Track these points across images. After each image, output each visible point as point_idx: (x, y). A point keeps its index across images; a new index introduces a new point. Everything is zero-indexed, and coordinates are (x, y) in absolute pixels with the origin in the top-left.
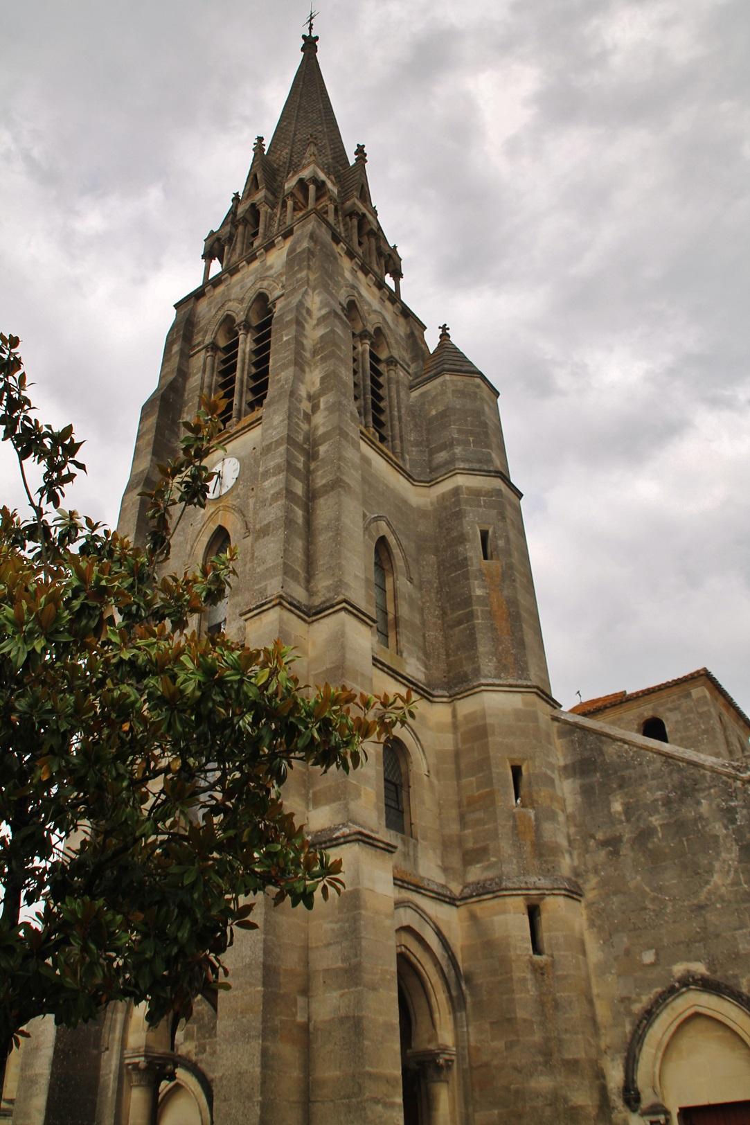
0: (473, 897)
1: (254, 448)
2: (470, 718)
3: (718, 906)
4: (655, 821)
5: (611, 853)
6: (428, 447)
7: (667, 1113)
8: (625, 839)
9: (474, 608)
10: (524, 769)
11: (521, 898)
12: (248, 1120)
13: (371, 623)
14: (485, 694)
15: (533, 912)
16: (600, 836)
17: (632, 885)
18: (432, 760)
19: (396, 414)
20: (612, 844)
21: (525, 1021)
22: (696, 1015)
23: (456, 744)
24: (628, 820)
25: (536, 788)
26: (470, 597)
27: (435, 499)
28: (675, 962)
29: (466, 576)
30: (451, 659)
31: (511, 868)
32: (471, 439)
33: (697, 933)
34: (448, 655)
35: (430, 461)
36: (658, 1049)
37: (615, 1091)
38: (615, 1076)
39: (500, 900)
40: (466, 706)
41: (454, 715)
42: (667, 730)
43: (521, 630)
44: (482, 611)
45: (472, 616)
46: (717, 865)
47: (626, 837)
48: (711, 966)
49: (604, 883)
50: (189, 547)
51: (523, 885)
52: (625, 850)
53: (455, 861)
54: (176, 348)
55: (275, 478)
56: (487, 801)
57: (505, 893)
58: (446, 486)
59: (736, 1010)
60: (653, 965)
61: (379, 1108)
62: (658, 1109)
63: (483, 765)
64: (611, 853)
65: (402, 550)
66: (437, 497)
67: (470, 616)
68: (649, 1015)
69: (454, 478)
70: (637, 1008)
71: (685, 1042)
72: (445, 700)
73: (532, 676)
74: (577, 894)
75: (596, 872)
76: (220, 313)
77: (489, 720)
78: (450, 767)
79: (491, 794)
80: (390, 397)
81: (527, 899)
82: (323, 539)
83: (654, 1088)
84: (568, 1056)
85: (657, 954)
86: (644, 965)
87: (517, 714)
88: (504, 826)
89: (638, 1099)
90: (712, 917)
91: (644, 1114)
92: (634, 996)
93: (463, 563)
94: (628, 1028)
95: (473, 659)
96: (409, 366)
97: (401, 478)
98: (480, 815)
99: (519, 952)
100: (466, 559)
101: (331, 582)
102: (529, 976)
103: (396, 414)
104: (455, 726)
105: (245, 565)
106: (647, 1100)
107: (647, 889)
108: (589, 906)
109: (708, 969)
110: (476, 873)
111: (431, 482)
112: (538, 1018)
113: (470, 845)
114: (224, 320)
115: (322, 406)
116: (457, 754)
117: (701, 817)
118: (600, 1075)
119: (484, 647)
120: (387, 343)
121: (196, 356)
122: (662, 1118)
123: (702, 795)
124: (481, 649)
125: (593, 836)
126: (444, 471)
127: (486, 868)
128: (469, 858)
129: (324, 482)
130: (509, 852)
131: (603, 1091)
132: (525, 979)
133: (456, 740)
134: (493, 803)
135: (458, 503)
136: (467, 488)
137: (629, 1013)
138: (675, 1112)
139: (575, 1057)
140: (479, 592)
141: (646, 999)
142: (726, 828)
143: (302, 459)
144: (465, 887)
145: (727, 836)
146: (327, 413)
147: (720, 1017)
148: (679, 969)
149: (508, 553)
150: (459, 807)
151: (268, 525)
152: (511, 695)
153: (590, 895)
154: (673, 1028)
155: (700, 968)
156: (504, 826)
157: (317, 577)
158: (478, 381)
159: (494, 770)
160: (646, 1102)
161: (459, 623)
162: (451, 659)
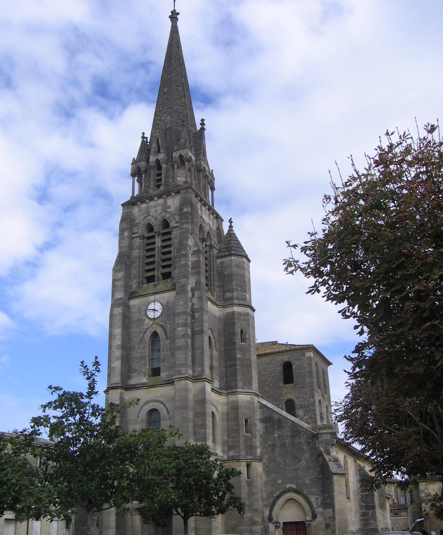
0: (230, 460)
1: (168, 302)
2: (233, 402)
3: (302, 469)
4: (287, 441)
5: (272, 449)
6: (223, 289)
7: (279, 523)
8: (277, 445)
9: (237, 362)
10: (249, 421)
11: (245, 462)
12: (88, 369)
13: (211, 382)
14: (239, 395)
15: (248, 466)
16: (269, 443)
17: (278, 460)
18: (220, 416)
19: (212, 273)
20: (273, 446)
21: (244, 498)
22: (291, 499)
23: (228, 410)
25: (252, 427)
26: (236, 357)
28: (287, 484)
29: (235, 349)
30: (227, 379)
31: (243, 453)
32: (240, 288)
33: (294, 476)
34: (226, 378)
35: (224, 295)
36: (279, 507)
37: (266, 517)
38: (267, 513)
39: (239, 463)
40: (232, 398)
41: (228, 400)
44: (239, 363)
45: (236, 365)
46: (303, 458)
47: (278, 445)
50: (142, 335)
51: (246, 459)
53: (226, 449)
55: (182, 328)
56: (237, 431)
57: (241, 461)
58: (229, 310)
59: (302, 498)
60: (281, 484)
62: (277, 522)
63: (237, 419)
64: (272, 449)
65: (214, 339)
66: (226, 313)
67: (235, 365)
68: (278, 497)
69: (233, 308)
70: (275, 495)
71: (287, 505)
72: (225, 394)
73: (254, 388)
74: (261, 460)
75: (267, 454)
77: (239, 404)
79: (239, 429)
80: (210, 264)
81: (247, 463)
82: (197, 352)
84: (255, 508)
86: (278, 483)
88: (242, 439)
89: (272, 520)
90: (299, 473)
91: (273, 523)
92: (274, 492)
93: (234, 344)
95: (235, 380)
96: (217, 245)
97: (214, 306)
98: (234, 435)
99: (244, 478)
100: (235, 342)
101: (201, 369)
103: (212, 273)
104: (228, 404)
105: (167, 351)
106: (275, 520)
108: (264, 464)
109: (296, 487)
110: (232, 453)
111: (224, 306)
112: (248, 497)
115: (196, 296)
116: (228, 413)
117: (300, 443)
123: (301, 436)
124: (238, 378)
127: (236, 452)
128: (230, 448)
130: (243, 448)
132: (244, 486)
133: (228, 409)
134: (239, 432)
135: (233, 318)
136: (238, 312)
137: (273, 496)
138: (282, 523)
139: (257, 508)
140: (239, 356)
141: (278, 493)
142: (307, 447)
143: (190, 319)
144: (228, 457)
145: (307, 450)
147: (297, 500)
148: (288, 486)
149: (249, 340)
150: (228, 431)
152: (246, 395)
153: (265, 461)
154: (284, 502)
155: (294, 486)
156: (242, 439)
157: (195, 366)
158: (245, 260)
159: (240, 421)
160: (274, 520)
161: (231, 367)
162: (227, 379)
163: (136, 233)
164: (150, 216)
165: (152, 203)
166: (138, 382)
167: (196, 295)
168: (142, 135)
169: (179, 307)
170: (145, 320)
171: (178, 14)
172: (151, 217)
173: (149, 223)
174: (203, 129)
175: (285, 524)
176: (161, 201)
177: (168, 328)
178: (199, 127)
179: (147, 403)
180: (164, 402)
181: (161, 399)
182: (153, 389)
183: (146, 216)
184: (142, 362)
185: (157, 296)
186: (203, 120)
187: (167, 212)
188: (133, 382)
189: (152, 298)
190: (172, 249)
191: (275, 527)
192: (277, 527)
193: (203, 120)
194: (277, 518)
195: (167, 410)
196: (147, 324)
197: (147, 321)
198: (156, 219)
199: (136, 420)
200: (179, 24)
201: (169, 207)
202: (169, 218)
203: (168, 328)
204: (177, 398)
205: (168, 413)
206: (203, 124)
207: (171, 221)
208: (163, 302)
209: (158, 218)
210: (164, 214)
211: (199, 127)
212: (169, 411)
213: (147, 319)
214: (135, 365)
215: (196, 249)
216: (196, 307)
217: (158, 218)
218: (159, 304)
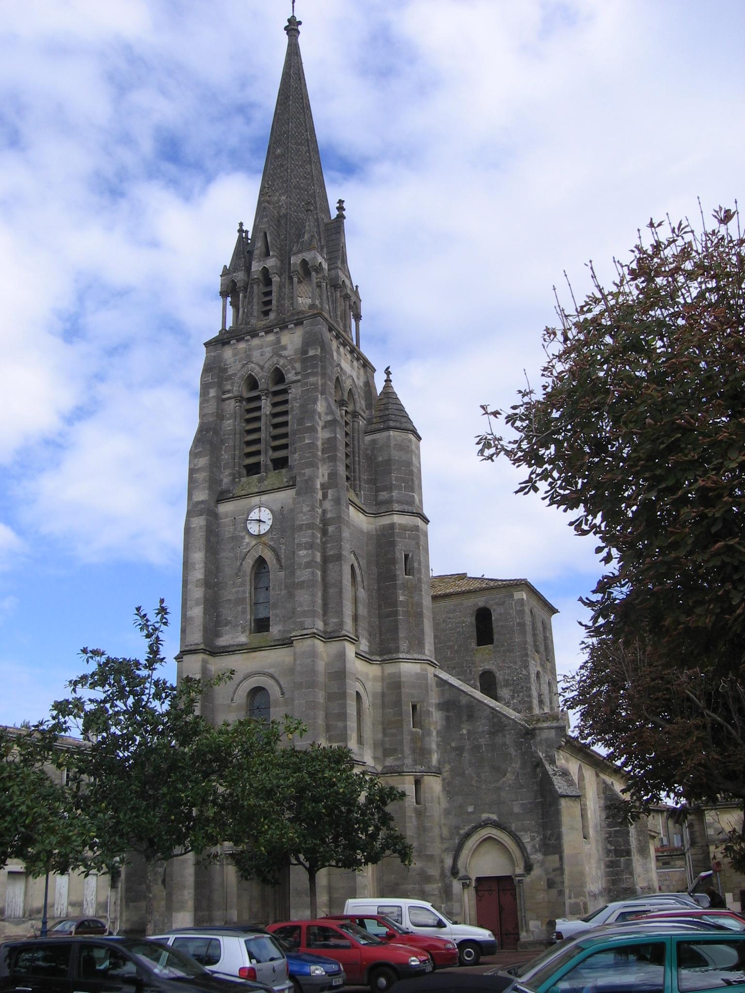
2: (392, 676)
4: (482, 741)
5: (457, 755)
7: (470, 879)
10: (418, 707)
15: (418, 783)
17: (467, 772)
20: (460, 750)
21: (410, 836)
22: (490, 838)
24: (469, 739)
25: (423, 718)
26: (396, 600)
27: (378, 527)
28: (483, 812)
29: (395, 586)
31: (408, 761)
34: (381, 635)
35: (376, 496)
38: (449, 862)
39: (402, 777)
40: (390, 669)
42: (493, 618)
43: (423, 623)
46: (509, 769)
48: (499, 816)
49: (452, 770)
52: (466, 754)
54: (212, 393)
58: (385, 521)
60: (472, 813)
61: (360, 878)
62: (467, 878)
63: (398, 703)
64: (457, 755)
65: (360, 569)
67: (396, 613)
68: (468, 835)
69: (391, 517)
70: (462, 832)
71: (483, 849)
73: (427, 652)
75: (449, 763)
76: (245, 369)
77: (403, 679)
78: (379, 701)
79: (401, 721)
80: (353, 444)
82: (332, 591)
83: (466, 868)
85: (475, 808)
87: (417, 674)
89: (457, 873)
90: (503, 794)
91: (460, 879)
92: (461, 827)
93: (394, 577)
94: (457, 841)
95: (396, 639)
96: (364, 412)
97: (361, 515)
98: (394, 731)
102: (414, 815)
104: (383, 678)
106: (462, 873)
107: (474, 776)
108: (443, 780)
109: (498, 818)
110: (390, 762)
113: (388, 746)
114: (248, 377)
115: (330, 497)
117: (505, 744)
118: (442, 861)
119: (402, 634)
120: (354, 399)
121: (227, 402)
122: (468, 881)
125: (449, 744)
126: (386, 510)
128: (387, 753)
129: (331, 553)
131: (442, 868)
133: (383, 686)
134: (402, 726)
135: (392, 535)
136: (400, 524)
137: (458, 834)
138: (474, 879)
140: (401, 598)
141: (467, 828)
142: (517, 751)
144: (384, 768)
146: (332, 503)
148: (485, 816)
151: (303, 582)
152: (414, 664)
153: (445, 774)
154: (478, 843)
155: (494, 817)
156: (407, 738)
158: (411, 436)
160: (461, 875)
163: (229, 392)
164: (252, 362)
165: (256, 342)
166: (232, 643)
167: (329, 496)
168: (238, 228)
169: (301, 515)
170: (243, 538)
171: (300, 23)
172: (253, 365)
173: (250, 374)
174: (341, 217)
175: (479, 880)
176: (271, 338)
177: (283, 551)
178: (334, 213)
179: (247, 677)
180: (276, 675)
181: (271, 671)
182: (257, 653)
183: (246, 364)
184: (240, 608)
185: (264, 498)
186: (341, 202)
187: (281, 356)
188: (223, 641)
189: (256, 500)
190: (289, 418)
191: (463, 886)
192: (465, 886)
193: (341, 202)
194: (466, 871)
195: (281, 688)
196: (248, 544)
197: (247, 539)
198: (262, 368)
199: (229, 706)
200: (301, 40)
201: (284, 348)
202: (284, 366)
203: (283, 551)
204: (298, 668)
205: (283, 694)
206: (341, 208)
207: (288, 371)
208: (274, 508)
209: (266, 366)
210: (275, 359)
211: (334, 213)
212: (285, 690)
213: (247, 537)
214: (228, 613)
215: (329, 418)
216: (329, 515)
217: (266, 366)
218: (268, 511)
